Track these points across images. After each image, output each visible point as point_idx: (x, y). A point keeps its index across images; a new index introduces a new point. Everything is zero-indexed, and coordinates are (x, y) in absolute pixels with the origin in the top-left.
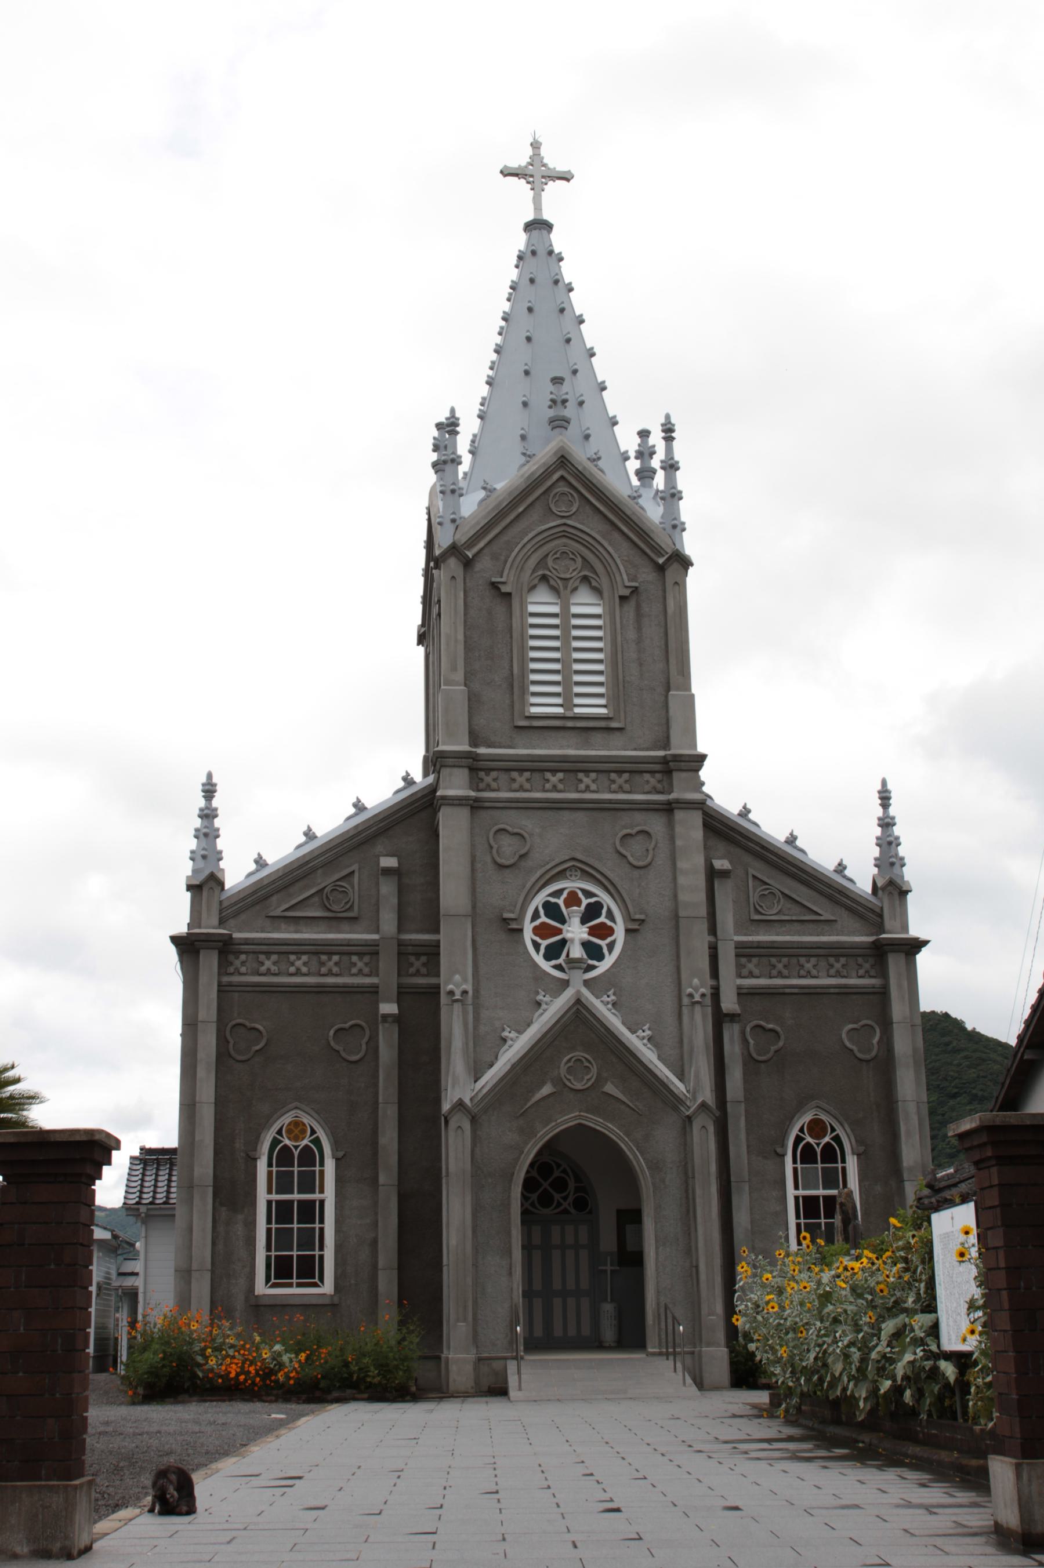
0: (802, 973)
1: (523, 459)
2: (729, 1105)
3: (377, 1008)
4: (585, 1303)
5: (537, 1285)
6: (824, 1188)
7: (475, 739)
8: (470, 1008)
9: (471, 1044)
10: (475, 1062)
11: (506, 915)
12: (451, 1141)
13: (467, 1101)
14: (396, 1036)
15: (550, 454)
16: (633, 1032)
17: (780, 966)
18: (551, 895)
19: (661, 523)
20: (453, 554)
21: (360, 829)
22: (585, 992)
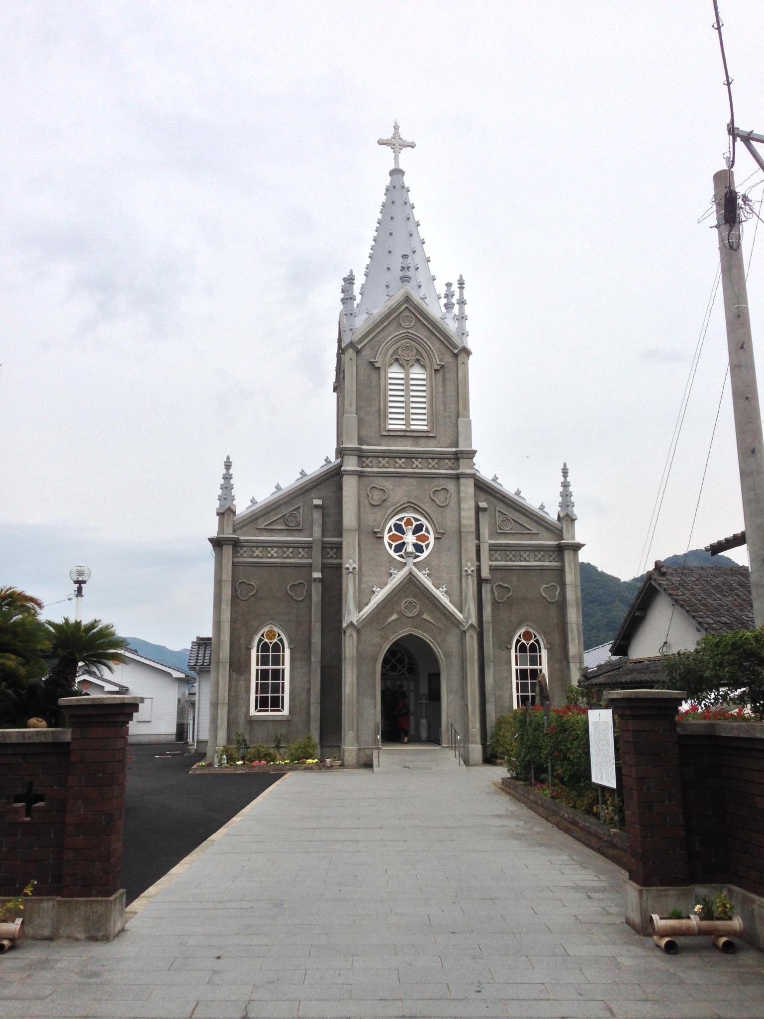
0: (522, 559)
2: (484, 624)
3: (311, 575)
6: (530, 665)
8: (357, 577)
11: (375, 530)
12: (346, 642)
13: (355, 622)
16: (438, 589)
17: (511, 556)
20: (351, 347)
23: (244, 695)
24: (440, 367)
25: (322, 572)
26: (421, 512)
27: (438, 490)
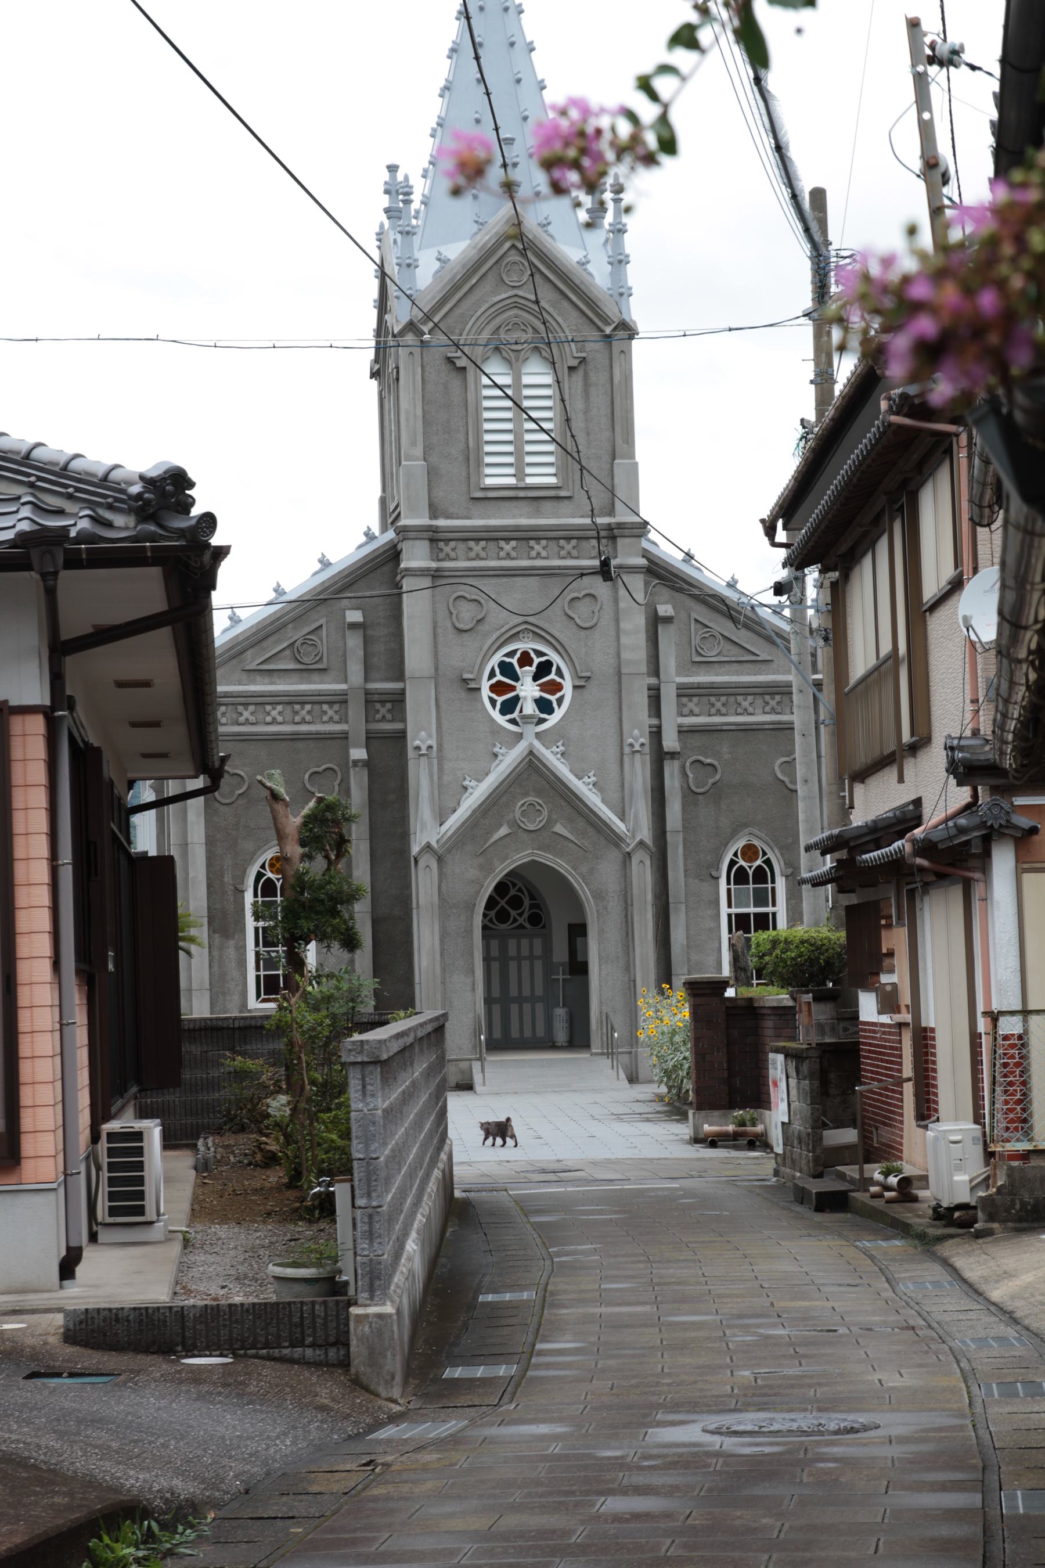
0: (739, 710)
1: (476, 227)
2: (668, 834)
3: (348, 754)
4: (540, 1007)
5: (496, 993)
6: (755, 906)
7: (434, 511)
8: (435, 761)
9: (436, 793)
10: (440, 808)
11: (466, 676)
12: (420, 879)
13: (434, 844)
14: (366, 778)
15: (502, 223)
16: (580, 778)
17: (718, 705)
18: (505, 655)
19: (609, 289)
20: (410, 330)
21: (326, 585)
22: (537, 744)
23: (235, 973)
24: (578, 360)
25: (367, 747)
26: (551, 643)
27: (578, 598)
